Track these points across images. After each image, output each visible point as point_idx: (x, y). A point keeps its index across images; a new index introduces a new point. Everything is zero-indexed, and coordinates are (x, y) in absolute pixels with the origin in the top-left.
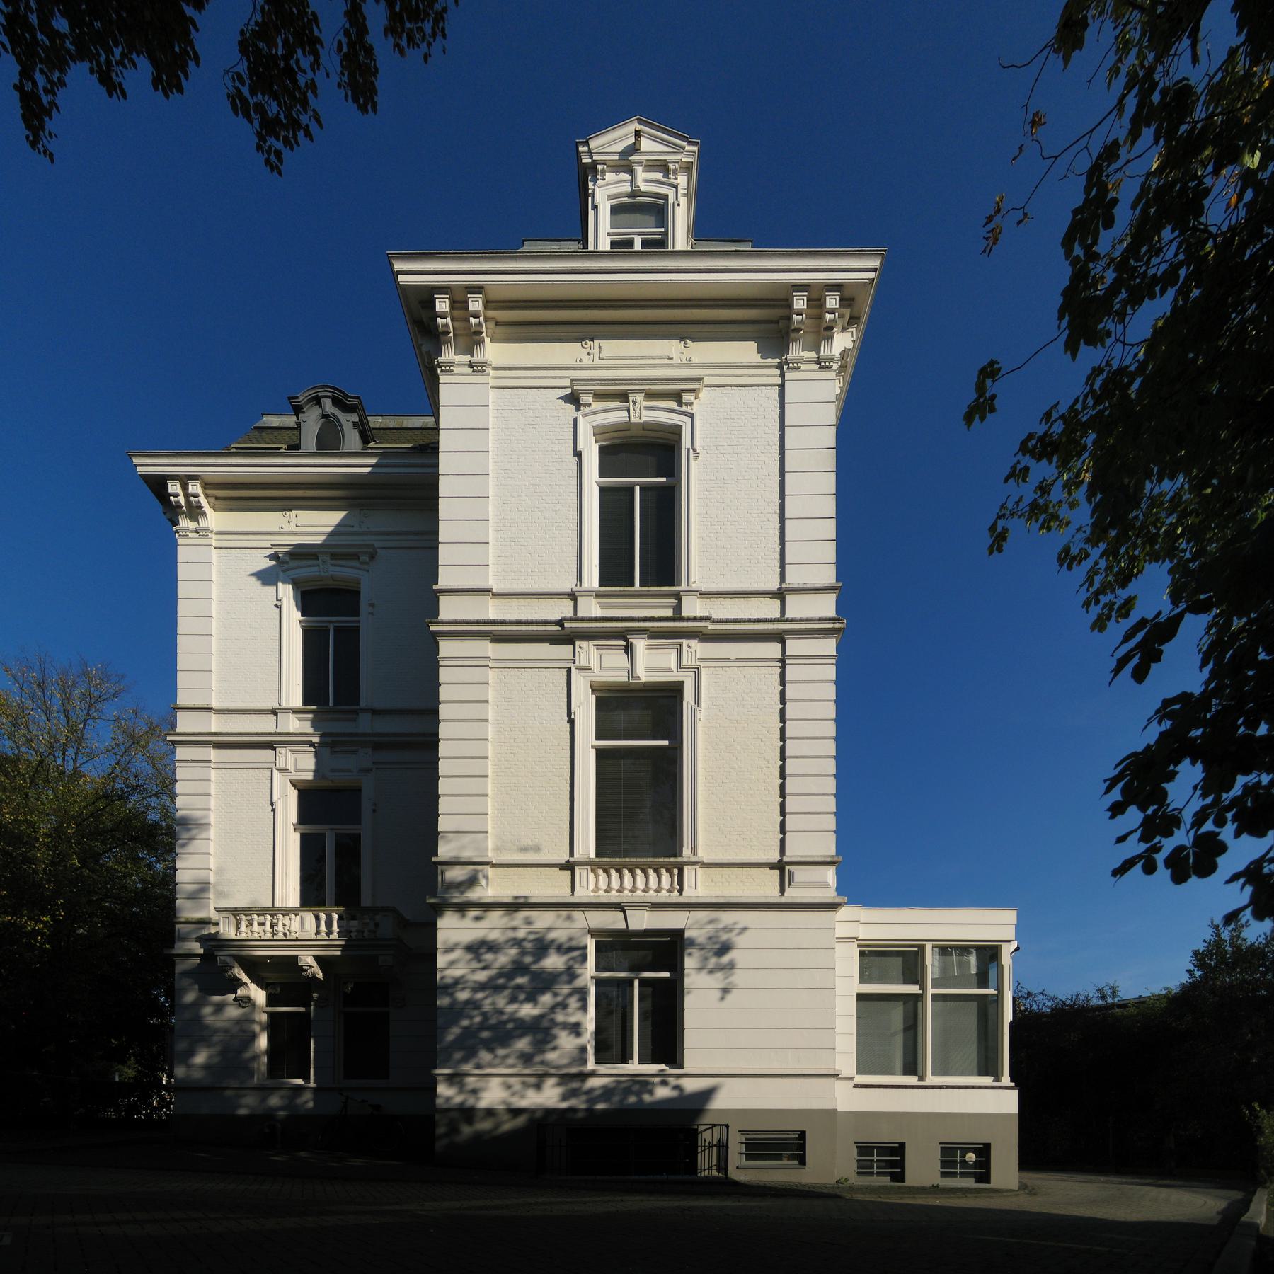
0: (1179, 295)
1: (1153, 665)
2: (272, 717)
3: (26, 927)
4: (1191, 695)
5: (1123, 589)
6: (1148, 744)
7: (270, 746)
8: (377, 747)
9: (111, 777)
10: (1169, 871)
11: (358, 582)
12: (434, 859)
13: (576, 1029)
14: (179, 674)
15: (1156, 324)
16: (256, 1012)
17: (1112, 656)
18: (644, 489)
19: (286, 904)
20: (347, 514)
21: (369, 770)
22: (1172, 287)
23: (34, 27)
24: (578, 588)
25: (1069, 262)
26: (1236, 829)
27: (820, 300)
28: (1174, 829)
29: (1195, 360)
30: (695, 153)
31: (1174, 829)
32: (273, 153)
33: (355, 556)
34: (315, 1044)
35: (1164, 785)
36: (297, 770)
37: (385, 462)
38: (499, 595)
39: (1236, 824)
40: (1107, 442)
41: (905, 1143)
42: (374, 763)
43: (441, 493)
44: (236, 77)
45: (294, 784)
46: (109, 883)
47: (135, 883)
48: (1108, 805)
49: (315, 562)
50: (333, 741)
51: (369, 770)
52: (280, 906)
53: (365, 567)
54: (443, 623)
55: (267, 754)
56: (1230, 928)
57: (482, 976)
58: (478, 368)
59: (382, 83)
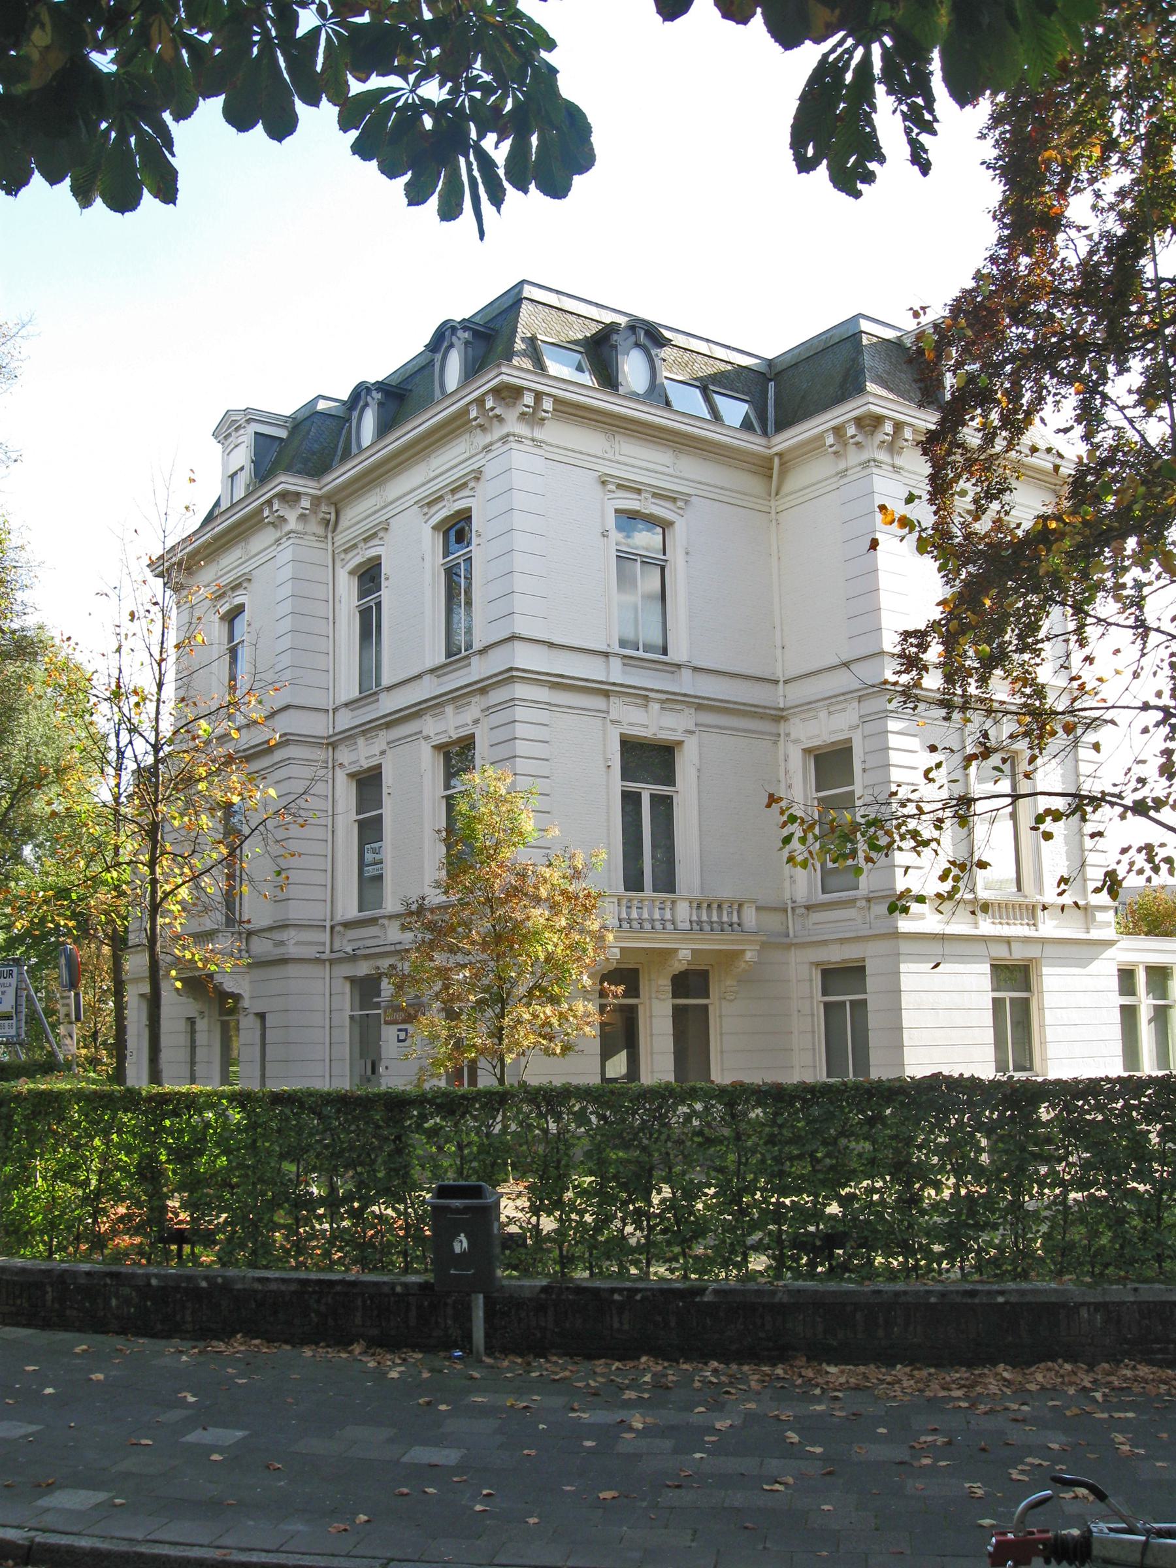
0: (378, 390)
1: (576, 178)
2: (600, 660)
3: (26, 1218)
4: (580, 173)
5: (558, 72)
6: (558, 72)
7: (606, 694)
8: (699, 707)
9: (488, 795)
10: (374, 163)
11: (624, 672)
12: (167, 116)
13: (40, 999)
14: (671, 1031)
15: (177, 989)
16: (900, 1079)
17: (262, 1016)
18: (1011, 999)
19: (862, 1062)
20: (765, 15)
21: (692, 732)
22: (1154, 999)
23: (440, 196)
24: (1169, 421)
25: (354, 134)
26: (297, 26)
27: (476, 1192)
28: (223, 97)
29: (992, 1113)
30: (324, 944)
31: (223, 97)
32: (506, 184)
33: (674, 500)
34: (315, 64)
35: (68, 181)
36: (332, 952)
37: (259, 517)
38: (814, 942)
39: (532, 187)
40: (128, 1208)
41: (52, 185)
42: (623, 643)
43: (871, 1063)
44: (339, 453)
45: (351, 776)
46: (1066, 358)
47: (1021, 337)
48: (953, 105)
49: (636, 497)
50: (667, 699)
51: (692, 732)
52: (1050, 1054)
53: (681, 512)
54: (922, 689)
55: (598, 702)
56: (1083, 168)
57: (1041, 572)
58: (896, 469)
59: (932, 156)
